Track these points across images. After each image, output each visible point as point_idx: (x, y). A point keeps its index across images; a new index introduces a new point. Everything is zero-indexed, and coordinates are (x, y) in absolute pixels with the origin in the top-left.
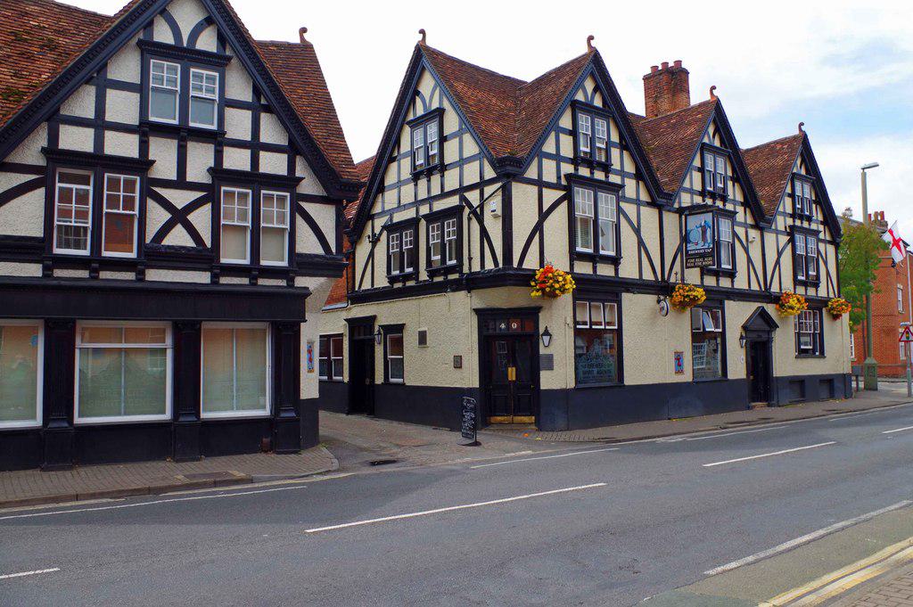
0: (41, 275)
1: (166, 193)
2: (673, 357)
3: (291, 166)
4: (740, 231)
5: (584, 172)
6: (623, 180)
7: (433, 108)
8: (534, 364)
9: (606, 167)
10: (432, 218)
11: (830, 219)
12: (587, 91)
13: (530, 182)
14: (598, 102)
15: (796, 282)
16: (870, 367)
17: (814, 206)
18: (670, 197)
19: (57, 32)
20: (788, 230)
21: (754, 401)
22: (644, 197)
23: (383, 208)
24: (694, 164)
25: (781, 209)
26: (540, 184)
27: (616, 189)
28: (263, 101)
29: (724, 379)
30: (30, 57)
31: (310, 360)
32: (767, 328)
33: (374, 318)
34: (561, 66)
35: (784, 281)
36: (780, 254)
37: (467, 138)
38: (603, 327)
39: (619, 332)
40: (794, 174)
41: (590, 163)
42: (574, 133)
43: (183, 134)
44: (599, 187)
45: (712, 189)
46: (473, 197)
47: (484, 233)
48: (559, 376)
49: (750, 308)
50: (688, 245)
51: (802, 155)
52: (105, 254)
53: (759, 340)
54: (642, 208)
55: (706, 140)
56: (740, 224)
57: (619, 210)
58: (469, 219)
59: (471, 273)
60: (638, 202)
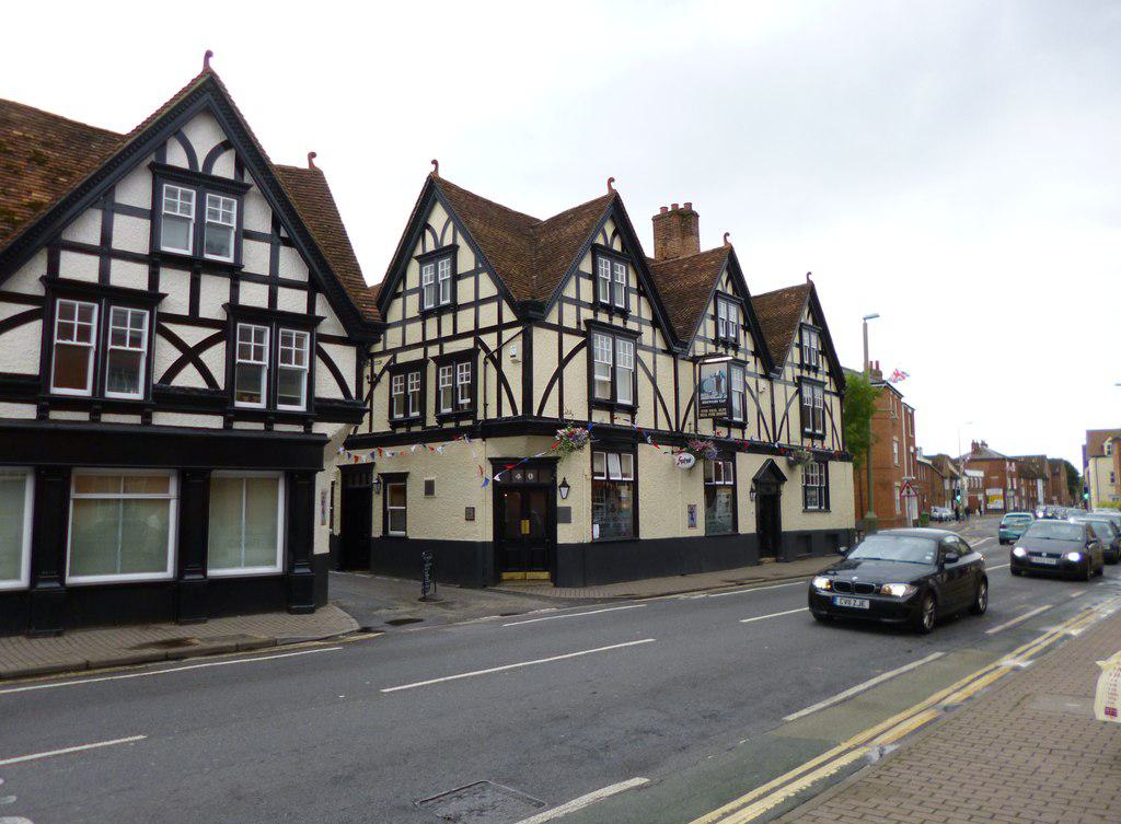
0: (34, 417)
1: (179, 330)
2: (686, 510)
3: (311, 305)
4: (751, 381)
5: (603, 318)
7: (445, 244)
8: (554, 516)
9: (624, 314)
10: (442, 360)
11: (836, 370)
12: (607, 234)
13: (550, 327)
14: (617, 246)
15: (804, 435)
18: (685, 345)
19: (45, 144)
22: (660, 344)
23: (385, 346)
25: (789, 359)
26: (561, 329)
27: (634, 336)
28: (283, 233)
30: (17, 173)
31: (323, 512)
32: (774, 480)
33: (371, 466)
34: (580, 207)
35: (792, 435)
36: (788, 405)
37: (484, 279)
39: (634, 485)
40: (802, 324)
41: (610, 309)
42: (594, 277)
43: (196, 267)
46: (490, 340)
47: (502, 379)
48: (577, 529)
52: (110, 395)
53: (769, 493)
55: (719, 288)
56: (751, 374)
57: (637, 358)
58: (486, 363)
59: (486, 421)
60: (654, 350)
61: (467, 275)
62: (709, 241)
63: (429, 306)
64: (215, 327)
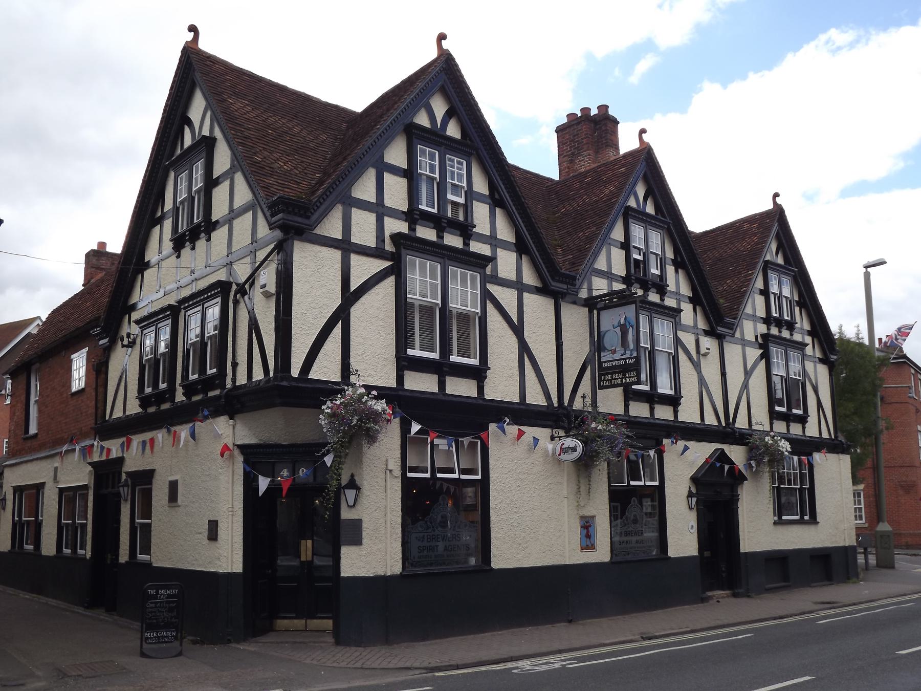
4: (688, 339)
5: (426, 233)
6: (494, 251)
9: (466, 230)
14: (650, 209)
15: (774, 416)
16: (884, 535)
17: (797, 309)
18: (571, 280)
20: (760, 341)
21: (711, 590)
22: (529, 278)
24: (756, 286)
26: (346, 246)
27: (479, 263)
29: (663, 556)
33: (120, 461)
36: (748, 374)
37: (239, 178)
38: (456, 476)
39: (484, 485)
40: (767, 263)
42: (410, 174)
44: (451, 258)
45: (777, 315)
49: (701, 452)
50: (602, 354)
51: (778, 237)
54: (526, 295)
55: (632, 203)
56: (686, 329)
59: (235, 387)
60: (519, 287)
62: (627, 143)
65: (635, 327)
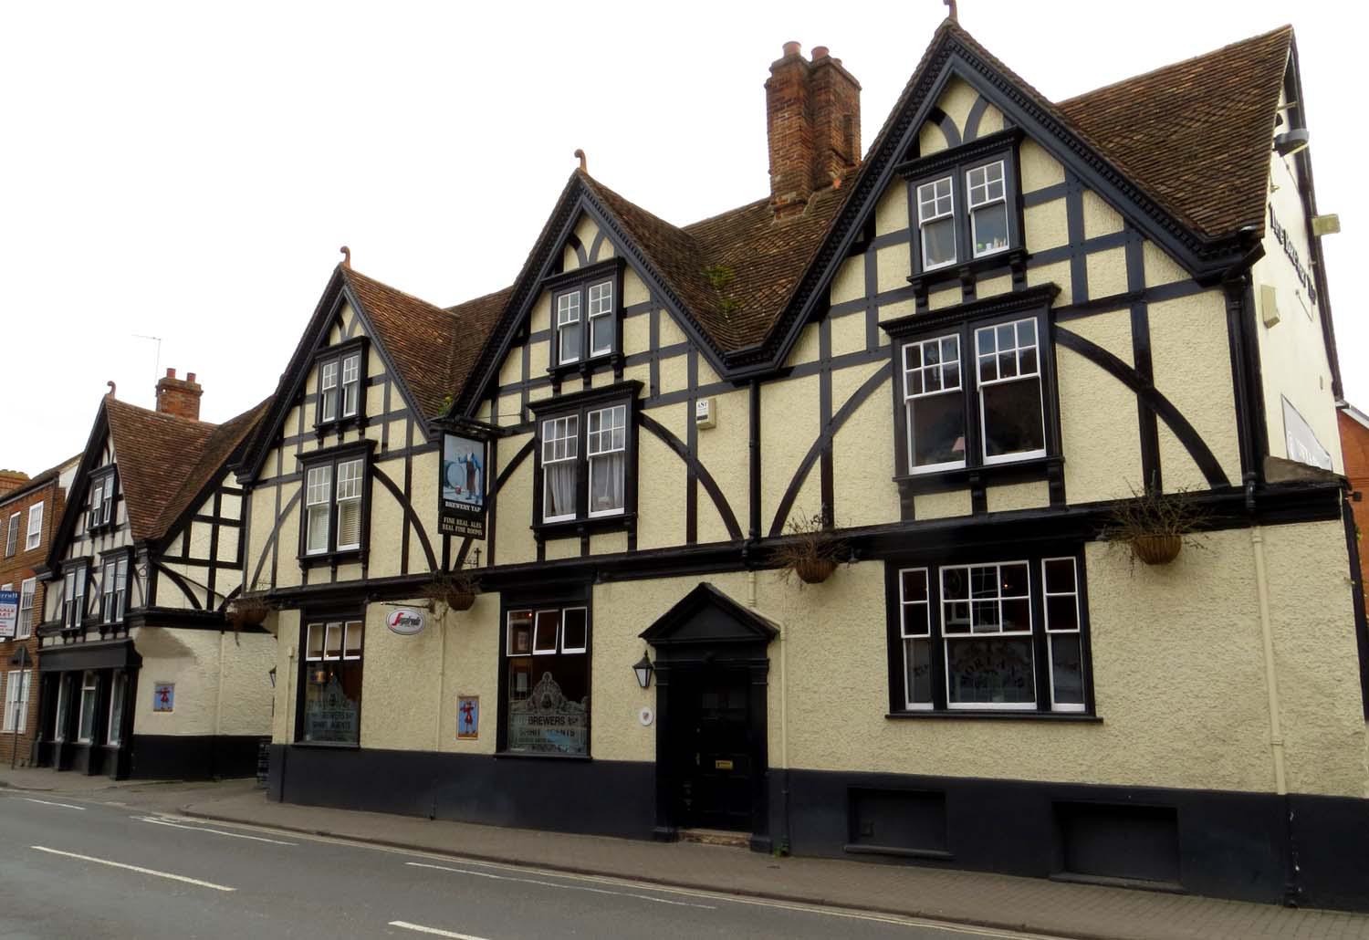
2: (453, 708)
36: (280, 519)
49: (667, 594)
61: (638, 310)
63: (329, 419)
64: (413, 425)
65: (482, 470)
